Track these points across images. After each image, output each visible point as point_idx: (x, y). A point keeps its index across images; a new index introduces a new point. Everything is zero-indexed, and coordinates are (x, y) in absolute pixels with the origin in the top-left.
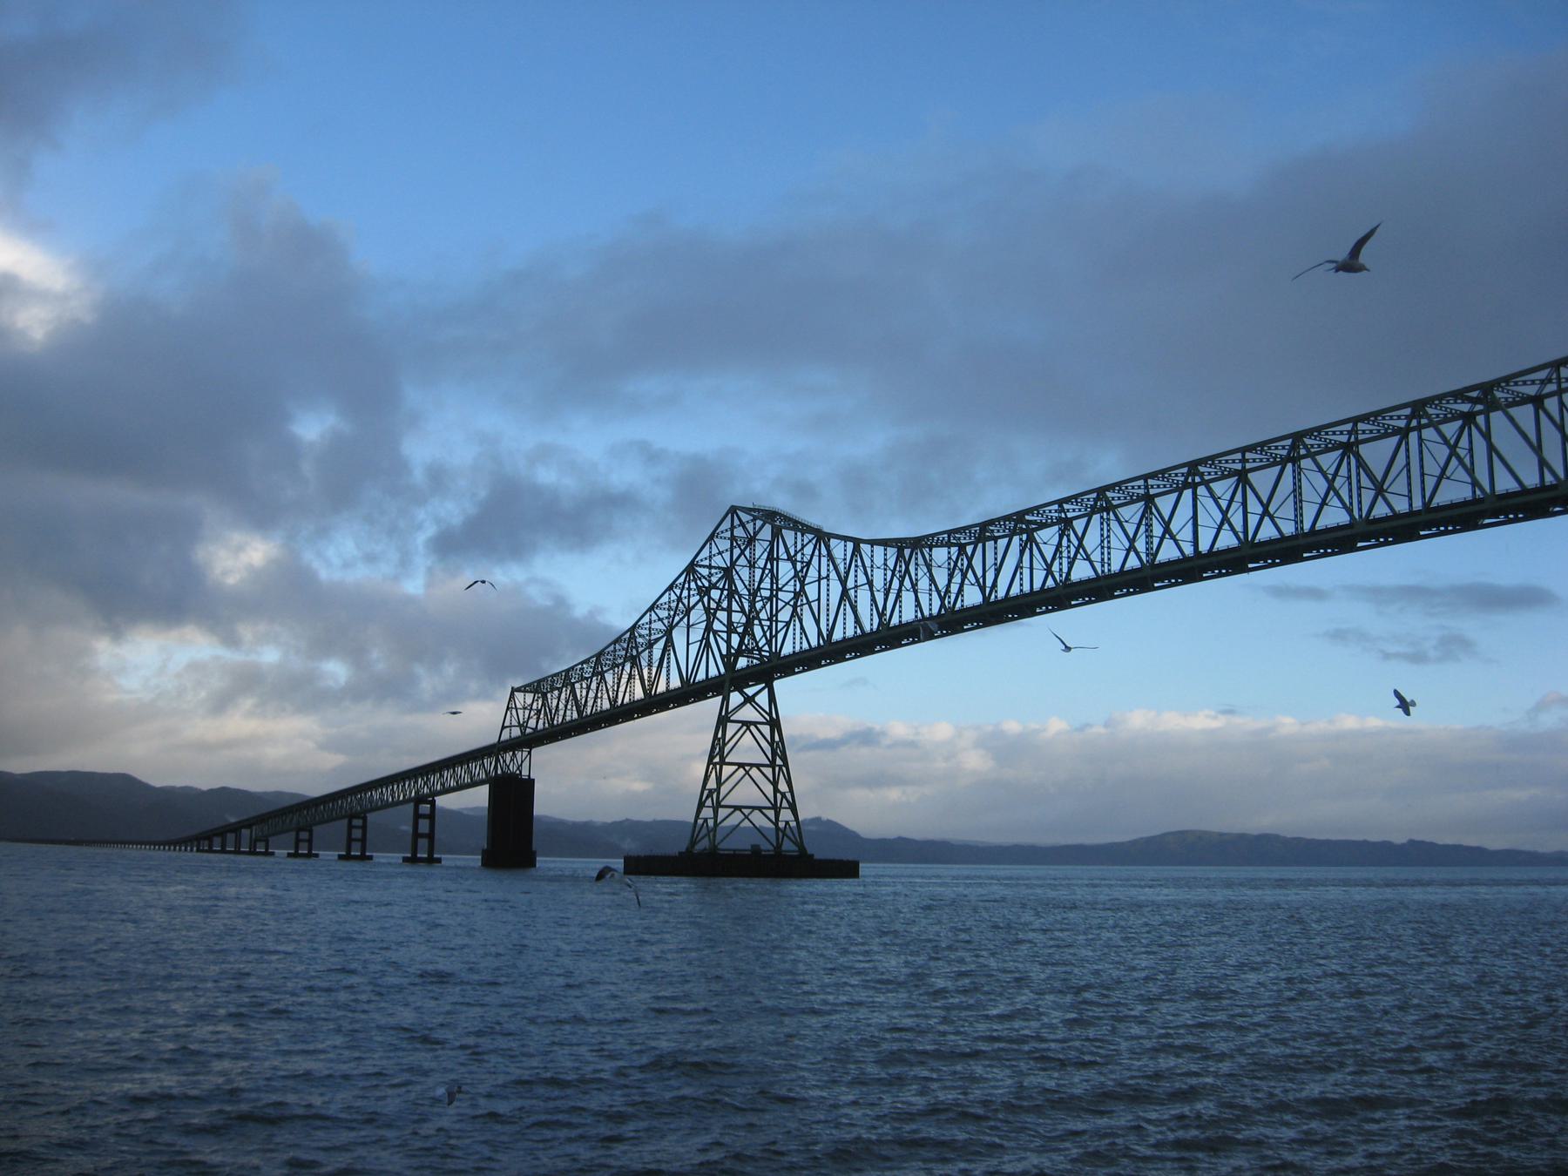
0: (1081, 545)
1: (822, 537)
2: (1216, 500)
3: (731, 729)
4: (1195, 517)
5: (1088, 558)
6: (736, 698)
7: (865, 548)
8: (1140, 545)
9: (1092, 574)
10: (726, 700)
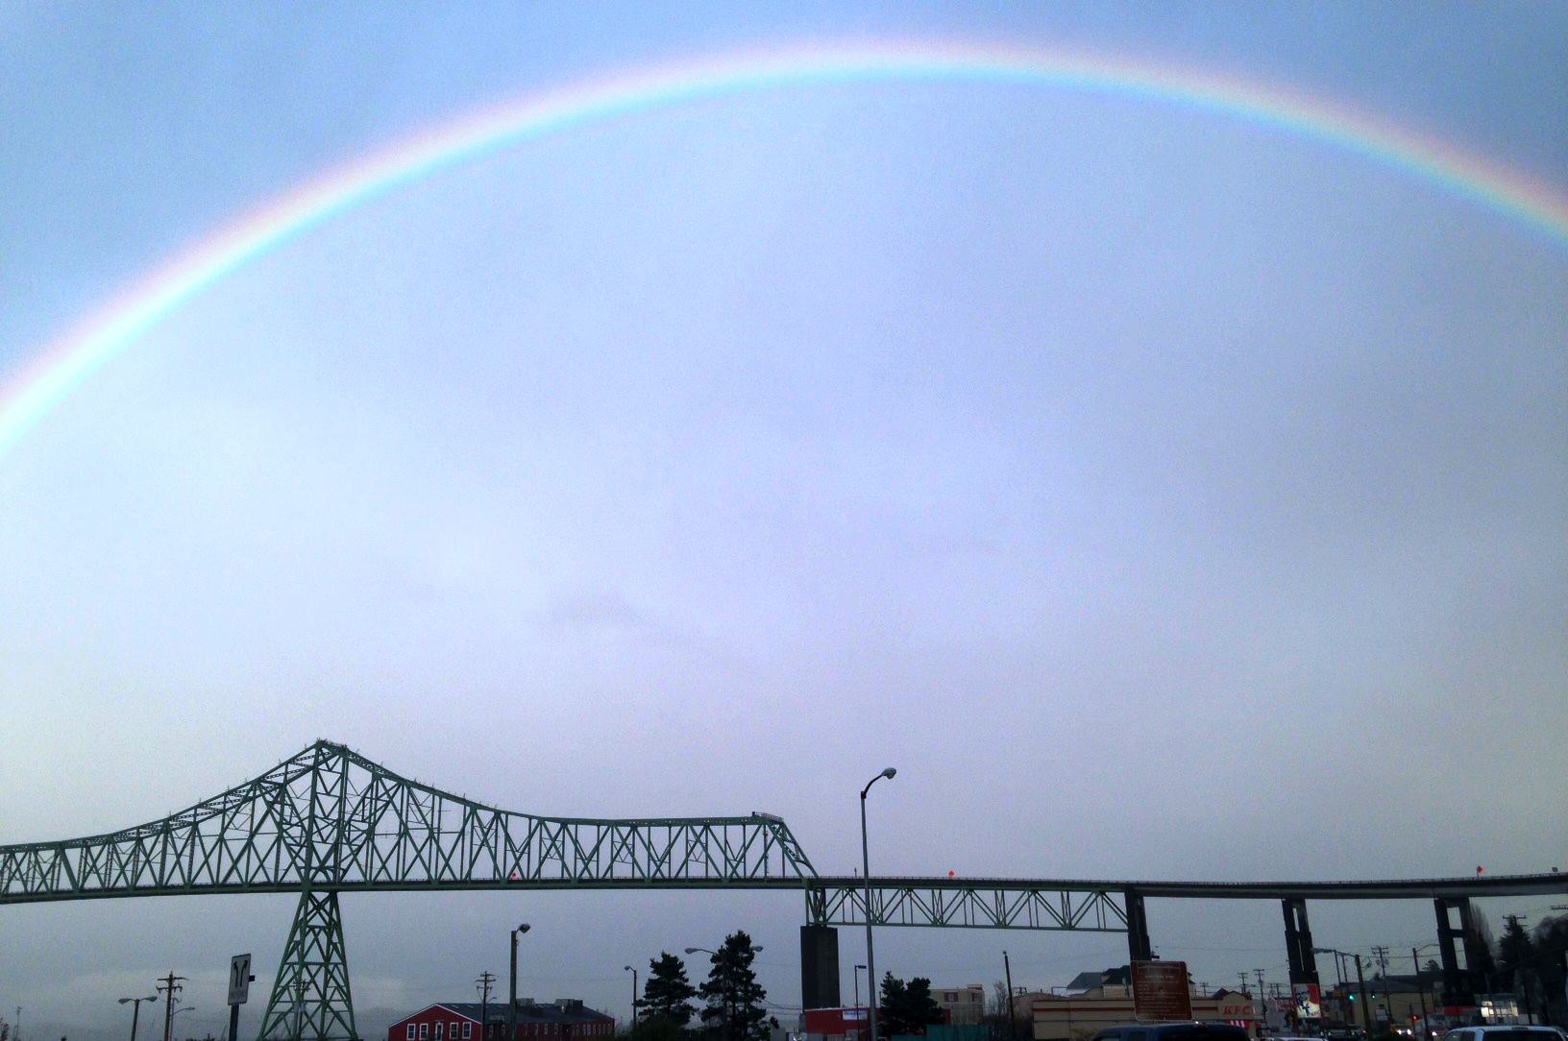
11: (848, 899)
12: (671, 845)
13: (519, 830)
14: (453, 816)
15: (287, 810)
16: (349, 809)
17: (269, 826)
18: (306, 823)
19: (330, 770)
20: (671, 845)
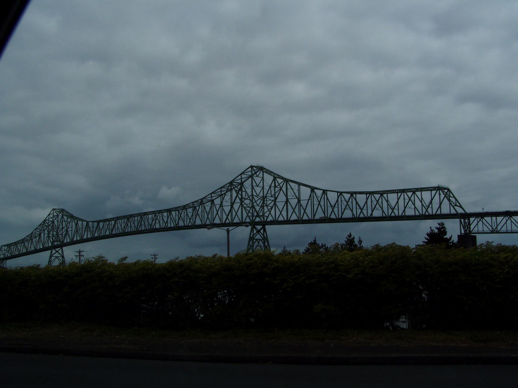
3: (53, 258)
6: (54, 251)
7: (91, 224)
11: (509, 221)
12: (432, 199)
13: (332, 197)
14: (305, 192)
15: (244, 193)
16: (265, 192)
17: (238, 200)
18: (251, 197)
19: (257, 176)
20: (432, 199)
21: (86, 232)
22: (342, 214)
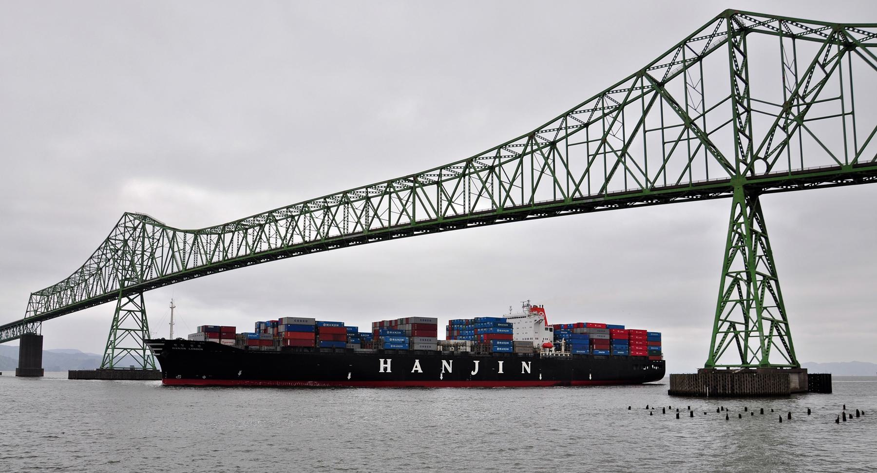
0: (334, 219)
1: (164, 227)
2: (400, 199)
4: (390, 208)
5: (337, 226)
6: (124, 300)
7: (180, 236)
8: (363, 220)
9: (339, 234)
10: (120, 301)
21: (192, 256)
22: (858, 155)
